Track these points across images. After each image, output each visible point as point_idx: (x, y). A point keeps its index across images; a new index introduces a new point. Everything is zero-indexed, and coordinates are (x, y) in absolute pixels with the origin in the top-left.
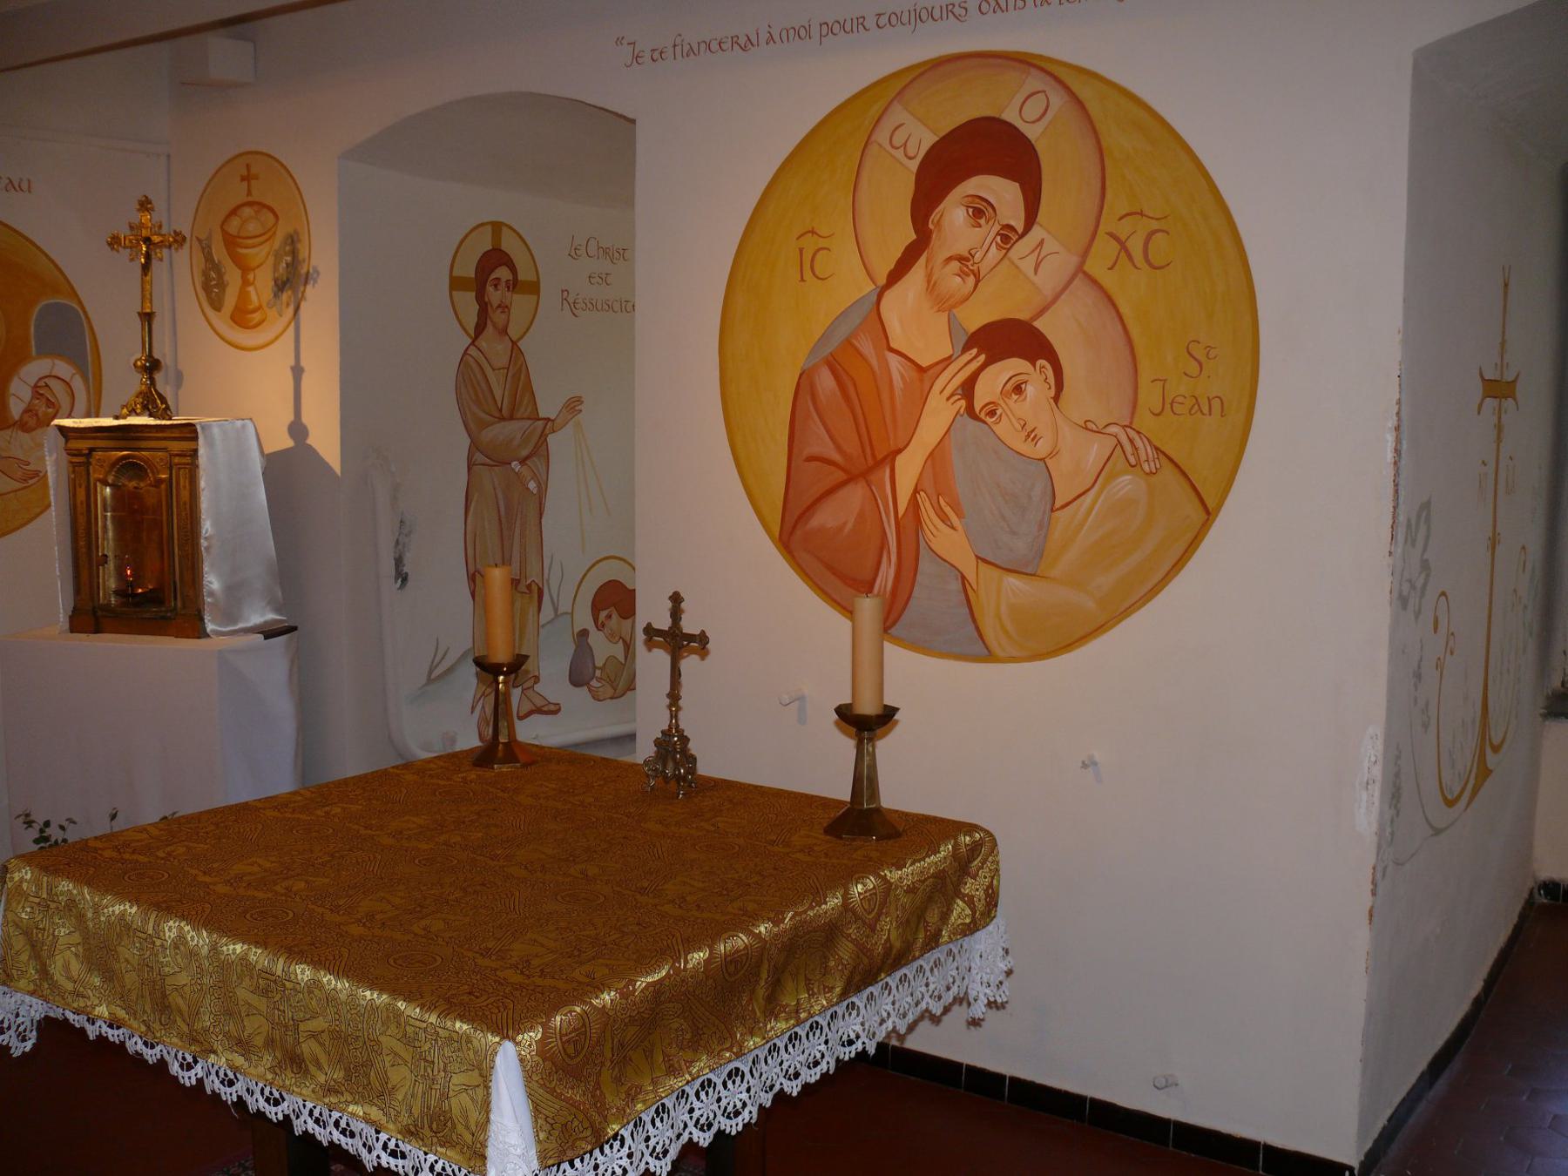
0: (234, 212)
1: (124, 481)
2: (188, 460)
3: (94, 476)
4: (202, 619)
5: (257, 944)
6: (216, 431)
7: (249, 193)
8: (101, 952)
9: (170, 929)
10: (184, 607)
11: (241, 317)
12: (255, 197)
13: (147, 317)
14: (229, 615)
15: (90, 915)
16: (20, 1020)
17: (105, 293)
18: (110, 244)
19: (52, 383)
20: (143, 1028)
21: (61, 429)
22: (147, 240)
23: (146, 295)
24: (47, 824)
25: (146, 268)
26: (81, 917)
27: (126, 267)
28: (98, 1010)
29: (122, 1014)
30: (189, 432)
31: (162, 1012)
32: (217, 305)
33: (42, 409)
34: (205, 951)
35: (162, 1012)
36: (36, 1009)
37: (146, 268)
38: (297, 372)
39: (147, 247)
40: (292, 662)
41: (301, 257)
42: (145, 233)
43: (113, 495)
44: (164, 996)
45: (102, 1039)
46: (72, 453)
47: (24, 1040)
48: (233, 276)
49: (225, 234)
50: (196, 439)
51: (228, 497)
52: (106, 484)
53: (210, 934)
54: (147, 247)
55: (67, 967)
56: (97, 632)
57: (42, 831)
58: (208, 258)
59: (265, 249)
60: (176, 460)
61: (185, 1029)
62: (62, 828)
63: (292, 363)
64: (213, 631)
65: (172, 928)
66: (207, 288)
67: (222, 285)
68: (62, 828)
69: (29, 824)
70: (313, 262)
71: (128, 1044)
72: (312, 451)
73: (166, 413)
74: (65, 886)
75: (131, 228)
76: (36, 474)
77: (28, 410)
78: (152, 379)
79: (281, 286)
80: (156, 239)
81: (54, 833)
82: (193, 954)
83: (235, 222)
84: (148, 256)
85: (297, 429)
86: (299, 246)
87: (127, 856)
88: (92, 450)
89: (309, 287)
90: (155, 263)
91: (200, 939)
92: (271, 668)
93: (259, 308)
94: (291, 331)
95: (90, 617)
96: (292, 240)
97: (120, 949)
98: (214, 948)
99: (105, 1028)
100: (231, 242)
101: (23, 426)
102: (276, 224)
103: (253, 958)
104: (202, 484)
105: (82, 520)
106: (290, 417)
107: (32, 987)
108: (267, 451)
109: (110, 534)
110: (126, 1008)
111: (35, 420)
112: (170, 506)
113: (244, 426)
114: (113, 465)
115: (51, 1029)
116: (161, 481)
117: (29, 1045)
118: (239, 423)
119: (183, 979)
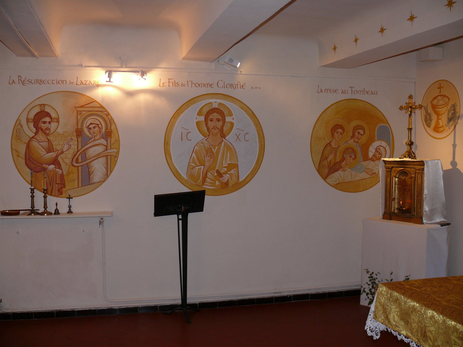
0: (435, 98)
1: (401, 177)
2: (421, 171)
3: (393, 174)
4: (422, 219)
5: (460, 323)
6: (430, 163)
7: (440, 92)
8: (405, 316)
9: (429, 313)
10: (417, 215)
11: (436, 129)
12: (442, 94)
13: (410, 129)
14: (430, 218)
15: (403, 304)
16: (377, 329)
17: (397, 122)
18: (400, 108)
19: (381, 148)
20: (417, 341)
21: (384, 161)
22: (411, 107)
23: (410, 123)
24: (373, 273)
25: (410, 115)
26: (400, 304)
27: (404, 115)
28: (402, 332)
29: (410, 335)
30: (422, 163)
31: (424, 337)
32: (429, 126)
33: (378, 155)
34: (441, 321)
35: (424, 337)
36: (382, 327)
37: (410, 115)
38: (454, 146)
39: (410, 108)
40: (448, 234)
41: (457, 111)
42: (410, 105)
43: (398, 180)
44: (425, 332)
45: (402, 340)
46: (386, 168)
47: (377, 335)
48: (434, 117)
49: (432, 104)
50: (424, 165)
51: (432, 182)
52: (396, 177)
53: (443, 317)
54: (410, 108)
55: (394, 317)
56: (390, 220)
57: (371, 275)
58: (427, 112)
59: (445, 108)
60: (417, 171)
61: (431, 344)
62: (376, 275)
63: (453, 143)
64: (426, 223)
65: (430, 313)
66: (426, 120)
67: (431, 120)
68: (376, 275)
69: (368, 272)
70: (461, 113)
71: (411, 344)
72: (458, 170)
73: (415, 157)
74: (396, 294)
75: (406, 103)
76: (375, 173)
77: (374, 155)
78: (411, 148)
79: (450, 120)
80: (413, 107)
81: (374, 276)
82: (436, 322)
83: (435, 101)
84: (411, 112)
85: (454, 163)
86: (456, 108)
87: (413, 288)
88: (392, 167)
89: (459, 120)
90: (413, 114)
91: (439, 318)
92: (442, 235)
93: (443, 126)
94: (453, 132)
95: (389, 215)
96: (454, 106)
97: (411, 315)
98: (444, 321)
99: (404, 338)
100: (434, 107)
101: (372, 160)
102: (448, 101)
103: (458, 327)
104: (425, 179)
105: (388, 187)
106: (451, 159)
107: (382, 321)
108: (444, 169)
109: (397, 192)
110: (412, 333)
111: (377, 157)
112: (415, 185)
113: (438, 162)
114: (398, 172)
115: (385, 334)
116: (413, 177)
117: (378, 337)
118: (436, 161)
119: (432, 329)
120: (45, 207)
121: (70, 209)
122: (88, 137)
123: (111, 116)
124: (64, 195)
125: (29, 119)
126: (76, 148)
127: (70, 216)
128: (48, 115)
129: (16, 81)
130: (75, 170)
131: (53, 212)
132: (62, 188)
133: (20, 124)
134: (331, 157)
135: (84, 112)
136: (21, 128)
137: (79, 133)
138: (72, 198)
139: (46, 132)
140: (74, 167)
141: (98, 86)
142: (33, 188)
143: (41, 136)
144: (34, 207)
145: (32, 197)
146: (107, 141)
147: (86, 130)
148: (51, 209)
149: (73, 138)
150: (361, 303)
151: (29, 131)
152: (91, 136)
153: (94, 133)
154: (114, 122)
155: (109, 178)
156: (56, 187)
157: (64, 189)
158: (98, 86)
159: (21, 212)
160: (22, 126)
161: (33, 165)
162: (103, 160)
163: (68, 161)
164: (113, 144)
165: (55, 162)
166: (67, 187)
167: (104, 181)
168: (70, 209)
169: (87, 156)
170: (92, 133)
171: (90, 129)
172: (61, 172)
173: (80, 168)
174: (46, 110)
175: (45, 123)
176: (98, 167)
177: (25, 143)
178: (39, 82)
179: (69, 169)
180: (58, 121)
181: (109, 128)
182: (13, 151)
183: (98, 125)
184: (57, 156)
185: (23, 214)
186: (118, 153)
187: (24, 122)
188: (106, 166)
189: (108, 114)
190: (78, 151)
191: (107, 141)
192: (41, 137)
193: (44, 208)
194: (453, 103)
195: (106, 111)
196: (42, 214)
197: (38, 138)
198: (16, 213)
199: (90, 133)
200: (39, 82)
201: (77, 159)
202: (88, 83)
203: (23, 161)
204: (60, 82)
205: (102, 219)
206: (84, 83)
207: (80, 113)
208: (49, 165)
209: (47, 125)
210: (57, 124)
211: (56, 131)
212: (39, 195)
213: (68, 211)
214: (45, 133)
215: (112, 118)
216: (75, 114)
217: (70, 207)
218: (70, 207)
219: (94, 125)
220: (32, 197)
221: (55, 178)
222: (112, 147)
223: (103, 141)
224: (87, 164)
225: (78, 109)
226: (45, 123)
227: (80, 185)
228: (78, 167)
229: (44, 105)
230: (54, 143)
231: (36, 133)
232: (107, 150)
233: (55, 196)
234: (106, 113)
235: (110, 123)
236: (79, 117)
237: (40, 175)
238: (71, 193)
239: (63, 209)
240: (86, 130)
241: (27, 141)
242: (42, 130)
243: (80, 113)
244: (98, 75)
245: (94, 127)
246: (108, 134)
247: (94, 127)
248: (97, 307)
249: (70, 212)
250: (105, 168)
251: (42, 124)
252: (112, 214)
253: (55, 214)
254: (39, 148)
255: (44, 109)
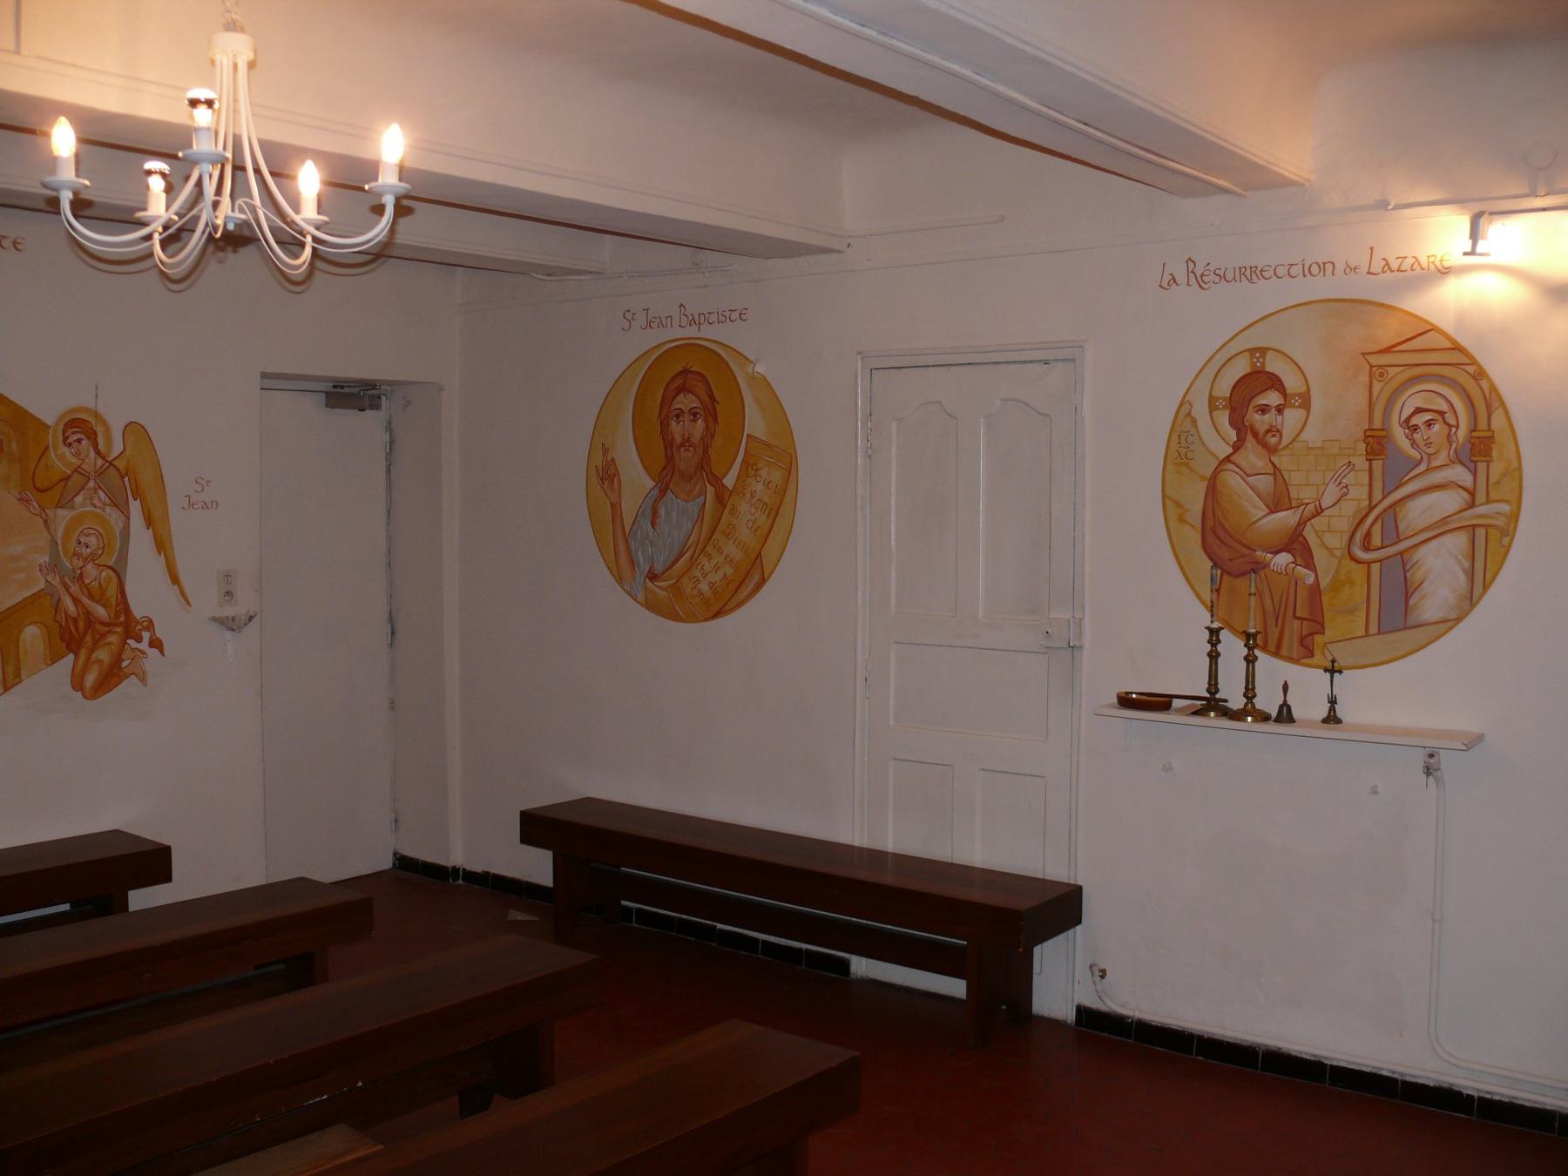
120: (1250, 693)
121: (1332, 709)
122: (1408, 458)
123: (1489, 380)
124: (1317, 659)
125: (1300, 407)
126: (1365, 496)
127: (1330, 732)
128: (1275, 383)
129: (1181, 277)
130: (1359, 572)
131: (1274, 714)
132: (1312, 634)
133: (1189, 415)
135: (1392, 371)
136: (1193, 431)
137: (1376, 443)
138: (1340, 672)
139: (1268, 442)
140: (1354, 565)
141: (1445, 272)
142: (1216, 625)
143: (1252, 456)
144: (1217, 691)
145: (1214, 656)
146: (1475, 475)
147: (1399, 434)
148: (1268, 701)
149: (1354, 460)
150: (132, 895)
151: (1216, 437)
152: (1415, 454)
153: (1428, 445)
154: (1502, 403)
155: (1477, 609)
156: (1294, 628)
157: (1318, 639)
158: (1445, 272)
159: (1176, 703)
160: (1194, 422)
161: (1227, 556)
162: (1457, 542)
163: (1337, 542)
164: (1498, 483)
165: (1295, 542)
166: (1330, 633)
167: (1459, 620)
168: (1332, 709)
169: (1401, 527)
170: (1421, 444)
171: (1415, 428)
172: (1311, 580)
173: (1375, 567)
174: (1268, 369)
175: (1264, 409)
176: (1440, 566)
177: (1203, 478)
178: (1251, 273)
179: (1337, 571)
180: (1305, 402)
181: (1482, 425)
182: (1170, 504)
183: (1442, 413)
184: (1302, 524)
185: (1181, 711)
186: (1514, 517)
187: (1201, 409)
188: (1467, 565)
189: (1480, 375)
190: (1371, 508)
191: (1475, 475)
192: (1252, 457)
193: (1245, 695)
195: (1474, 362)
196: (1237, 716)
197: (1243, 464)
198: (1158, 703)
199: (1413, 443)
200: (1251, 273)
201: (1368, 535)
202: (1406, 265)
203: (1195, 537)
204: (1315, 269)
205: (1431, 756)
206: (1394, 266)
207: (1381, 375)
208: (1276, 553)
209: (1269, 418)
210: (1301, 413)
211: (1302, 437)
212: (1233, 648)
213: (1325, 714)
214: (1265, 446)
215: (1494, 389)
216: (1364, 378)
217: (1333, 701)
218: (1333, 701)
219: (1428, 416)
220: (1214, 656)
221: (1292, 596)
222: (1493, 496)
223: (1460, 474)
224: (1401, 553)
225: (1374, 360)
226: (1264, 409)
227: (1373, 629)
228: (1369, 563)
229: (1263, 351)
230: (1294, 478)
231: (1237, 447)
232: (1472, 505)
233: (1290, 659)
234: (1471, 369)
235: (1488, 406)
236: (1377, 386)
237: (1249, 584)
238: (1341, 653)
239: (1309, 707)
240: (1399, 434)
241: (1208, 472)
242: (1255, 435)
243: (1381, 375)
244: (1442, 233)
245: (1429, 424)
246: (1479, 449)
247: (1429, 424)
248: (1399, 1069)
249: (1332, 719)
250: (1464, 570)
251: (1257, 416)
252: (1473, 742)
253: (1278, 720)
254: (1246, 495)
255: (1263, 364)
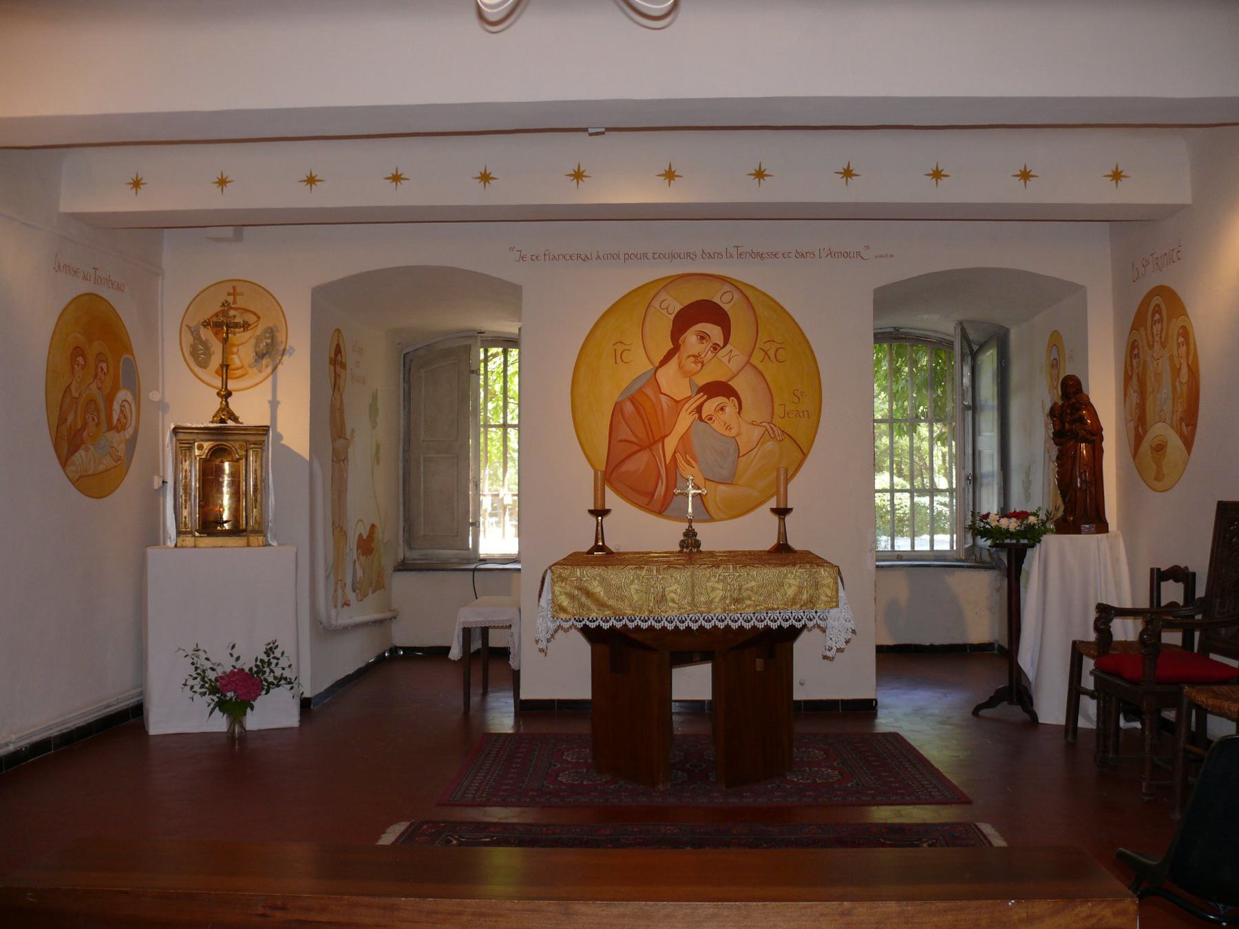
41: (279, 340)
46: (180, 441)
63: (270, 398)
66: (194, 353)
79: (260, 356)
89: (285, 358)
93: (242, 367)
134: (71, 418)
194: (271, 325)
